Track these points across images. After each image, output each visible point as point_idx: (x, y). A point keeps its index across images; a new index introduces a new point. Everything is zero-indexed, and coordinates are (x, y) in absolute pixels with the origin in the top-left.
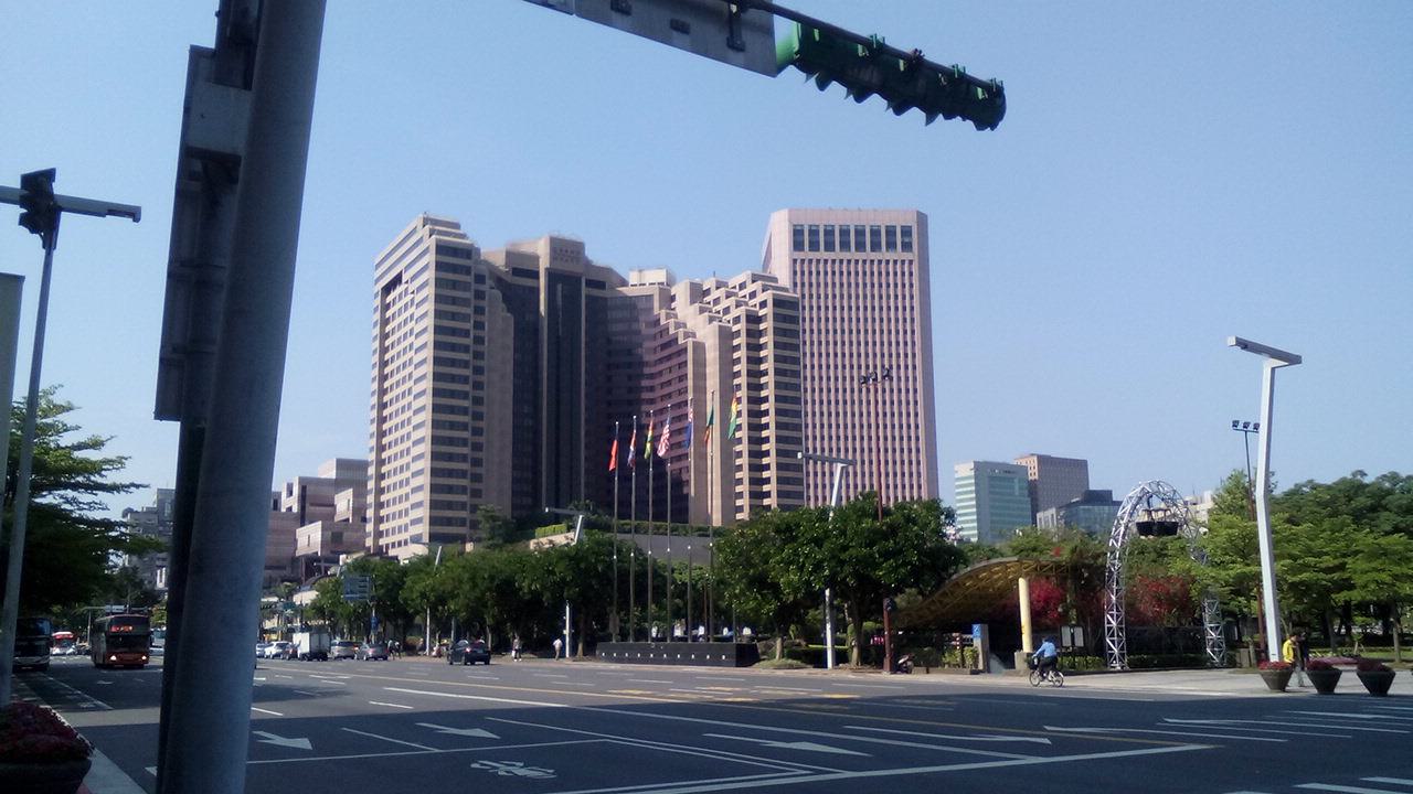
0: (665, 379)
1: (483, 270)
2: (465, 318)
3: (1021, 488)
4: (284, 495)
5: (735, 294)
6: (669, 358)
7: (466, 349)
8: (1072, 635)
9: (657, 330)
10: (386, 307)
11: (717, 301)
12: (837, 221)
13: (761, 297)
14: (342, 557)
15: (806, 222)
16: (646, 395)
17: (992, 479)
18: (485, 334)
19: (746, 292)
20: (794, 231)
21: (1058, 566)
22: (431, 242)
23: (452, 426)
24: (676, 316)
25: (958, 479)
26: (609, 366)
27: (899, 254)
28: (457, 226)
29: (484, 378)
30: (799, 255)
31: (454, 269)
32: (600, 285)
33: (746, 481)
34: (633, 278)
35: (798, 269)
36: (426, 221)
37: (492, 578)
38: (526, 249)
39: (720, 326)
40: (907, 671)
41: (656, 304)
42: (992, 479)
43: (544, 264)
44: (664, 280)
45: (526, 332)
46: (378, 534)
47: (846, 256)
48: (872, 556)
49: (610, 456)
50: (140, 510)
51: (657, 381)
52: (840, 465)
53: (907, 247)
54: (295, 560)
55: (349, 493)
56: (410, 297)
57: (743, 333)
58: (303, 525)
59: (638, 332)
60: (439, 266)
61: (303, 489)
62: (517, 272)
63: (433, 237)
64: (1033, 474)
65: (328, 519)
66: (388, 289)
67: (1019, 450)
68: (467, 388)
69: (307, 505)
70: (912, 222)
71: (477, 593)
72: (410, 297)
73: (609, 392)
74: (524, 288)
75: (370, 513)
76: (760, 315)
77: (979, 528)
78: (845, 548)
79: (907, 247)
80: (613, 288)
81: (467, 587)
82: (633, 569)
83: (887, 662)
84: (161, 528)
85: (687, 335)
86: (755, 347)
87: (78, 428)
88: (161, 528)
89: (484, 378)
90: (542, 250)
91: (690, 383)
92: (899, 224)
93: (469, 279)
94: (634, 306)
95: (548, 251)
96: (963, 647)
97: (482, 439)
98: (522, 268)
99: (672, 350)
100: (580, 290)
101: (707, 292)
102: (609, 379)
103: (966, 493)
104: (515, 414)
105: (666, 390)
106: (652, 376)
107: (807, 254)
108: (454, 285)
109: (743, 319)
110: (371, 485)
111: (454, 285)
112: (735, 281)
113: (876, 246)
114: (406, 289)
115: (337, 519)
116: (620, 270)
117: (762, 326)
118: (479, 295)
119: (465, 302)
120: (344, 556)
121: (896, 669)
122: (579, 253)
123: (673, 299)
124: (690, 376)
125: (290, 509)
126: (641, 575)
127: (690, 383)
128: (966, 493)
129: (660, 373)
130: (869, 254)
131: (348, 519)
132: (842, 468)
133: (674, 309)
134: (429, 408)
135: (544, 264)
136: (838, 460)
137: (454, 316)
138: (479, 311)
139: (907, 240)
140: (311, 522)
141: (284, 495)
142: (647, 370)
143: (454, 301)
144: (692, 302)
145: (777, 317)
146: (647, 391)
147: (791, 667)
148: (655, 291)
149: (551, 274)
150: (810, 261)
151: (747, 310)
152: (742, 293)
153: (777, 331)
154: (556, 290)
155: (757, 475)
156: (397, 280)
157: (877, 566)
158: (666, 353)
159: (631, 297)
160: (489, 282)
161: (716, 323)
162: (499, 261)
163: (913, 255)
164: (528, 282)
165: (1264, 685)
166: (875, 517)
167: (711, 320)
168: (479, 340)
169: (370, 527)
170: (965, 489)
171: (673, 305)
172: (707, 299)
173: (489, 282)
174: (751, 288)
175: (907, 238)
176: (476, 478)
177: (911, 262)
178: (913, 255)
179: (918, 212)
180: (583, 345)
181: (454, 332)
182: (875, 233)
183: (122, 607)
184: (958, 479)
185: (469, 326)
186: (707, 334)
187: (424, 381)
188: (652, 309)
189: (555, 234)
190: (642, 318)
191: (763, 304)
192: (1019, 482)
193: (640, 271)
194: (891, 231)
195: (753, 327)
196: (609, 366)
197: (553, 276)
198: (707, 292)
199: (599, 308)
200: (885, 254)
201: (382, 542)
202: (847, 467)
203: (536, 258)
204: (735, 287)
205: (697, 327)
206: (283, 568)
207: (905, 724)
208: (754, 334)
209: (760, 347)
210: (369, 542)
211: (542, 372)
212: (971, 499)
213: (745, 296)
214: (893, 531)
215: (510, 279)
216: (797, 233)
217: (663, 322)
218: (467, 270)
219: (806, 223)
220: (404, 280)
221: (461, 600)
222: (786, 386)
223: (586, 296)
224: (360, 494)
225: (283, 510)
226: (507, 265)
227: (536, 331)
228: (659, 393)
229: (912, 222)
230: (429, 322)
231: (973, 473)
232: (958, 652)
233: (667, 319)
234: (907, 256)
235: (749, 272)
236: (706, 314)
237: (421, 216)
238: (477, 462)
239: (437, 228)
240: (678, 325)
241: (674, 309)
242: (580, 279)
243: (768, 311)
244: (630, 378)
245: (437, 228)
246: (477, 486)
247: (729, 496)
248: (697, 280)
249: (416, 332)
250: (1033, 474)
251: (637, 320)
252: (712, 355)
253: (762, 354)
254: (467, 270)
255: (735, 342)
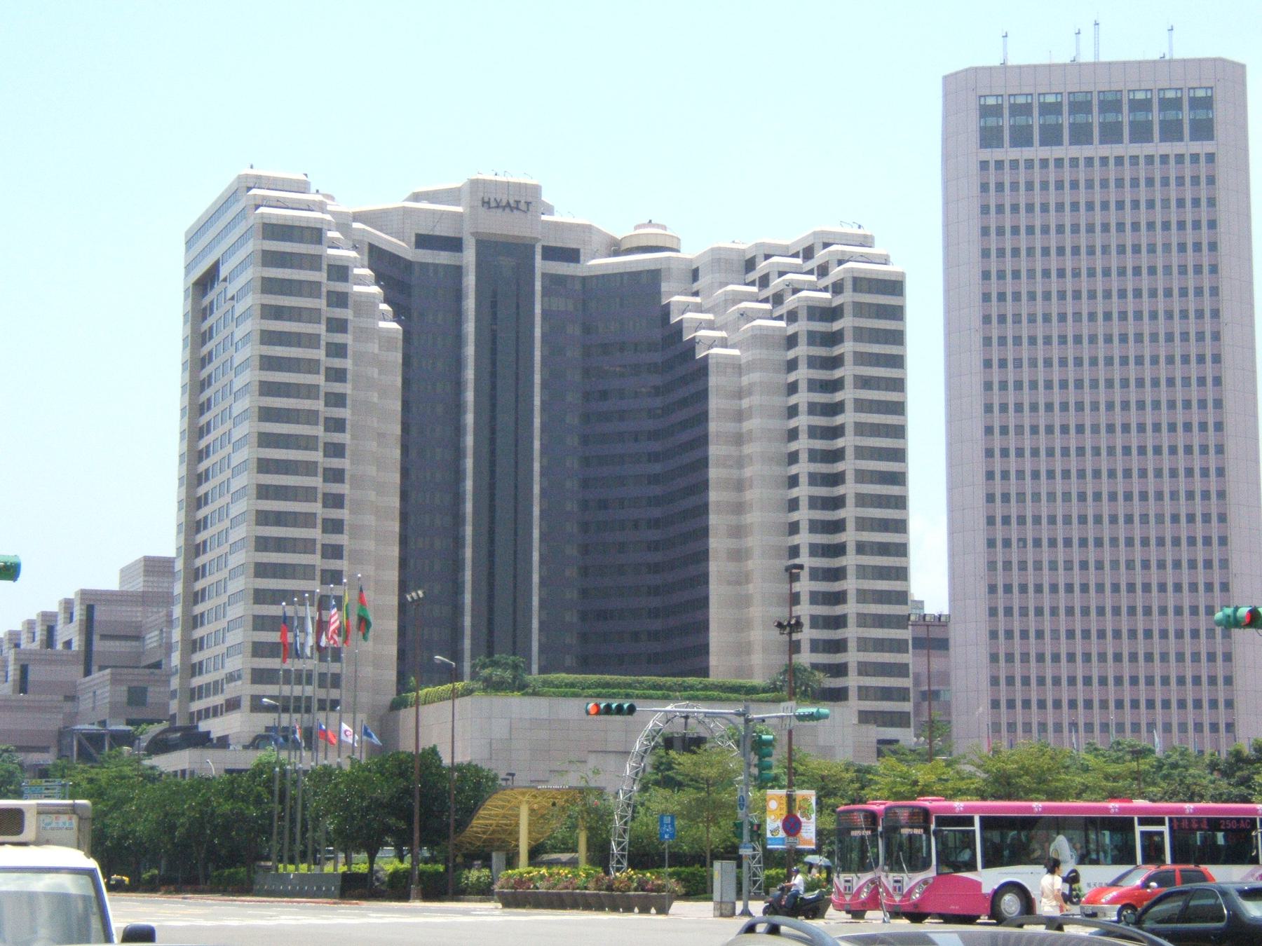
61: (90, 610)
69: (96, 638)
76: (834, 305)
107: (1008, 153)
125: (68, 644)
150: (1104, 161)
156: (214, 269)
207: (299, 201)
218: (902, 622)
225: (59, 646)
242: (533, 247)
254: (902, 622)
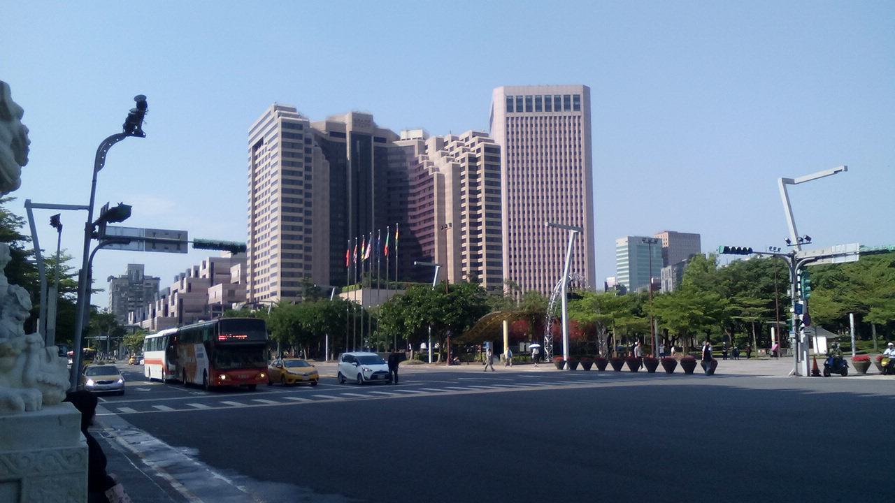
0: (421, 196)
1: (310, 135)
2: (299, 165)
3: (657, 252)
4: (201, 268)
5: (462, 145)
6: (423, 183)
7: (300, 183)
8: (525, 346)
9: (418, 166)
10: (255, 158)
11: (452, 149)
12: (534, 93)
13: (478, 146)
14: (234, 304)
15: (514, 94)
16: (410, 206)
17: (642, 248)
18: (312, 173)
19: (469, 143)
20: (507, 99)
21: (523, 314)
22: (278, 121)
23: (293, 228)
24: (428, 158)
25: (618, 248)
26: (389, 188)
27: (572, 113)
28: (294, 110)
29: (311, 200)
30: (510, 115)
31: (293, 136)
32: (383, 140)
33: (468, 257)
34: (403, 135)
35: (510, 124)
36: (276, 108)
37: (290, 321)
38: (338, 120)
39: (453, 165)
40: (457, 364)
41: (416, 151)
42: (642, 248)
43: (349, 129)
44: (421, 136)
45: (338, 169)
46: (254, 291)
47: (539, 114)
48: (441, 311)
49: (346, 259)
50: (118, 277)
51: (417, 197)
52: (572, 232)
53: (577, 108)
54: (206, 307)
55: (239, 266)
56: (268, 152)
57: (467, 168)
58: (212, 286)
59: (406, 168)
60: (284, 135)
61: (212, 264)
62: (333, 134)
63: (280, 117)
64: (665, 243)
65: (226, 282)
66: (256, 147)
67: (657, 226)
68: (302, 206)
69: (214, 274)
70: (580, 92)
71: (284, 328)
72: (268, 152)
73: (389, 204)
74: (338, 143)
75: (249, 279)
77: (630, 278)
78: (430, 308)
79: (577, 108)
80: (391, 142)
81: (279, 325)
82: (355, 316)
83: (448, 360)
84: (131, 288)
85: (434, 170)
86: (473, 176)
87: (74, 268)
88: (131, 288)
89: (311, 200)
90: (347, 121)
91: (435, 198)
92: (572, 93)
93: (302, 141)
94: (402, 152)
95: (351, 121)
96: (482, 351)
97: (311, 236)
98: (336, 131)
99: (425, 178)
100: (371, 144)
101: (446, 143)
102: (389, 196)
103: (623, 256)
104: (331, 219)
105: (422, 203)
106: (414, 195)
107: (515, 114)
108: (293, 145)
109: (467, 160)
110: (249, 262)
111: (293, 145)
112: (462, 136)
113: (558, 108)
114: (266, 148)
115: (232, 281)
116: (394, 129)
117: (478, 164)
118: (308, 151)
119: (299, 156)
120: (235, 304)
121: (452, 363)
122: (370, 121)
123: (426, 147)
124: (435, 194)
125: (204, 276)
126: (366, 318)
127: (435, 198)
128: (623, 256)
129: (419, 193)
130: (553, 113)
131: (238, 282)
132: (574, 233)
133: (427, 154)
134: (280, 218)
135: (349, 129)
136: (572, 227)
137: (293, 164)
138: (308, 160)
139: (577, 103)
140: (217, 284)
141: (201, 268)
142: (411, 191)
143: (293, 155)
144: (438, 149)
145: (486, 158)
146: (411, 203)
147: (416, 363)
148: (415, 143)
149: (353, 135)
151: (469, 154)
152: (467, 144)
153: (486, 166)
154: (356, 143)
155: (474, 253)
157: (442, 315)
158: (422, 180)
159: (401, 147)
160: (314, 142)
161: (450, 162)
162: (322, 128)
163: (581, 113)
164: (339, 140)
165: (556, 368)
166: (445, 293)
167: (448, 160)
168: (308, 177)
169: (249, 287)
170: (622, 254)
171: (427, 151)
172: (446, 147)
173: (314, 142)
174: (472, 140)
175: (578, 102)
176: (308, 258)
177: (579, 117)
178: (581, 113)
179: (584, 86)
180: (373, 177)
181: (293, 173)
182: (557, 99)
183: (106, 337)
184: (618, 248)
185: (302, 169)
186: (446, 169)
187: (276, 203)
188: (413, 154)
189: (355, 111)
190: (408, 159)
191: (479, 150)
192: (656, 249)
193: (407, 131)
194: (567, 99)
195: (473, 164)
196: (389, 188)
197: (354, 136)
198: (446, 143)
199: (382, 154)
200: (563, 113)
201: (256, 296)
202: (577, 233)
203: (344, 125)
204: (462, 140)
205: (439, 164)
206: (199, 311)
208: (473, 168)
209: (477, 176)
210: (248, 296)
211: (348, 194)
212: (626, 260)
213: (468, 146)
214: (453, 299)
215: (329, 138)
216: (509, 101)
217: (420, 162)
219: (514, 95)
220: (264, 143)
221: (277, 332)
222: (492, 199)
223: (375, 147)
224: (244, 268)
225: (201, 277)
226: (326, 130)
227: (345, 169)
228: (418, 204)
229: (580, 92)
230: (279, 168)
231: (627, 244)
232: (480, 356)
233: (422, 160)
234: (577, 113)
235: (471, 131)
236: (445, 157)
237: (273, 105)
238: (308, 249)
239: (283, 112)
240: (429, 164)
241: (427, 154)
243: (481, 154)
244: (401, 196)
245: (283, 112)
246: (308, 263)
247: (459, 265)
248: (440, 136)
249: (271, 173)
250: (665, 243)
251: (405, 161)
252: (448, 182)
253: (478, 180)
254: (300, 137)
255: (462, 174)
